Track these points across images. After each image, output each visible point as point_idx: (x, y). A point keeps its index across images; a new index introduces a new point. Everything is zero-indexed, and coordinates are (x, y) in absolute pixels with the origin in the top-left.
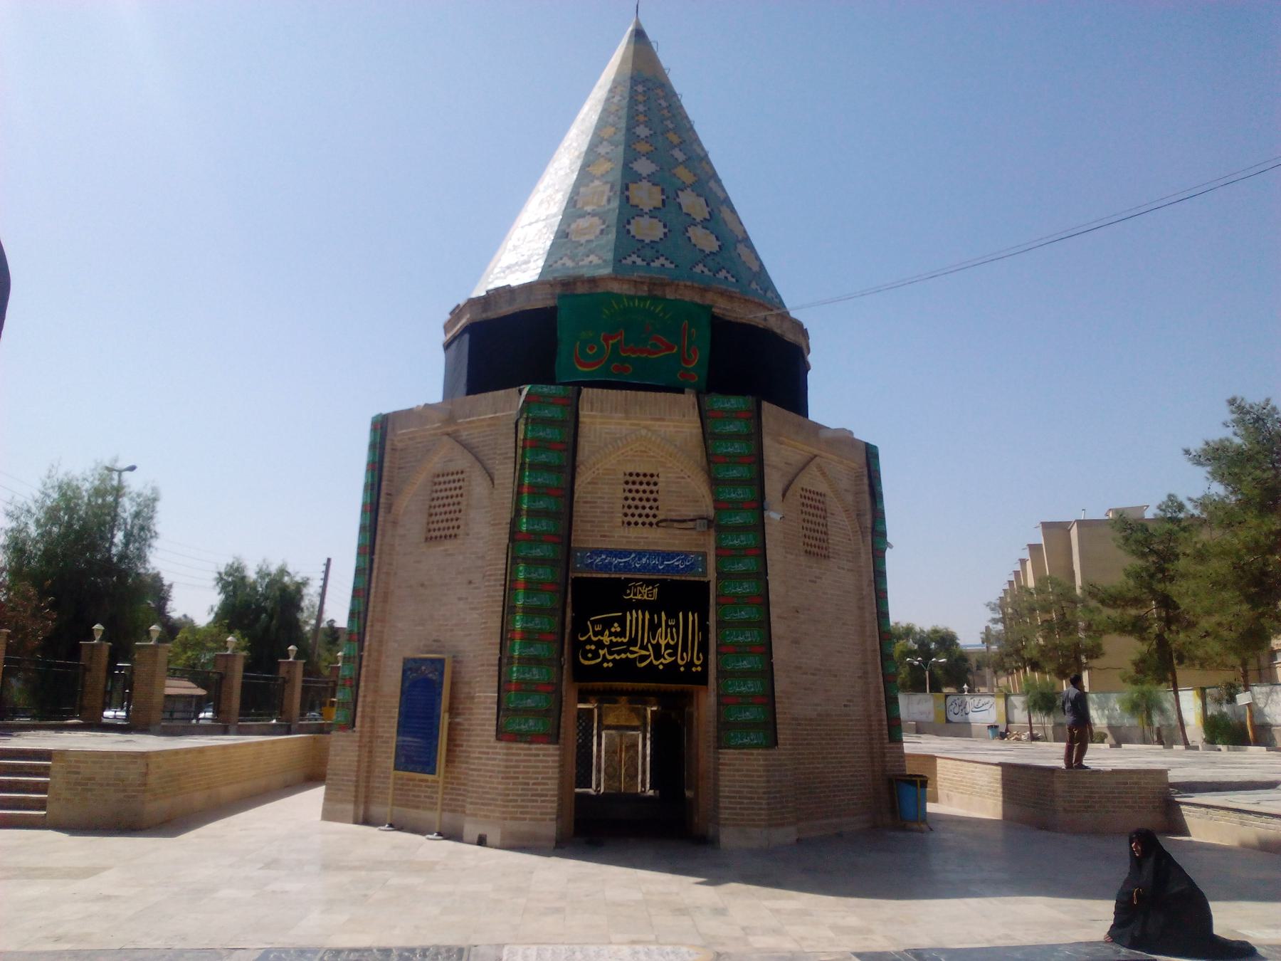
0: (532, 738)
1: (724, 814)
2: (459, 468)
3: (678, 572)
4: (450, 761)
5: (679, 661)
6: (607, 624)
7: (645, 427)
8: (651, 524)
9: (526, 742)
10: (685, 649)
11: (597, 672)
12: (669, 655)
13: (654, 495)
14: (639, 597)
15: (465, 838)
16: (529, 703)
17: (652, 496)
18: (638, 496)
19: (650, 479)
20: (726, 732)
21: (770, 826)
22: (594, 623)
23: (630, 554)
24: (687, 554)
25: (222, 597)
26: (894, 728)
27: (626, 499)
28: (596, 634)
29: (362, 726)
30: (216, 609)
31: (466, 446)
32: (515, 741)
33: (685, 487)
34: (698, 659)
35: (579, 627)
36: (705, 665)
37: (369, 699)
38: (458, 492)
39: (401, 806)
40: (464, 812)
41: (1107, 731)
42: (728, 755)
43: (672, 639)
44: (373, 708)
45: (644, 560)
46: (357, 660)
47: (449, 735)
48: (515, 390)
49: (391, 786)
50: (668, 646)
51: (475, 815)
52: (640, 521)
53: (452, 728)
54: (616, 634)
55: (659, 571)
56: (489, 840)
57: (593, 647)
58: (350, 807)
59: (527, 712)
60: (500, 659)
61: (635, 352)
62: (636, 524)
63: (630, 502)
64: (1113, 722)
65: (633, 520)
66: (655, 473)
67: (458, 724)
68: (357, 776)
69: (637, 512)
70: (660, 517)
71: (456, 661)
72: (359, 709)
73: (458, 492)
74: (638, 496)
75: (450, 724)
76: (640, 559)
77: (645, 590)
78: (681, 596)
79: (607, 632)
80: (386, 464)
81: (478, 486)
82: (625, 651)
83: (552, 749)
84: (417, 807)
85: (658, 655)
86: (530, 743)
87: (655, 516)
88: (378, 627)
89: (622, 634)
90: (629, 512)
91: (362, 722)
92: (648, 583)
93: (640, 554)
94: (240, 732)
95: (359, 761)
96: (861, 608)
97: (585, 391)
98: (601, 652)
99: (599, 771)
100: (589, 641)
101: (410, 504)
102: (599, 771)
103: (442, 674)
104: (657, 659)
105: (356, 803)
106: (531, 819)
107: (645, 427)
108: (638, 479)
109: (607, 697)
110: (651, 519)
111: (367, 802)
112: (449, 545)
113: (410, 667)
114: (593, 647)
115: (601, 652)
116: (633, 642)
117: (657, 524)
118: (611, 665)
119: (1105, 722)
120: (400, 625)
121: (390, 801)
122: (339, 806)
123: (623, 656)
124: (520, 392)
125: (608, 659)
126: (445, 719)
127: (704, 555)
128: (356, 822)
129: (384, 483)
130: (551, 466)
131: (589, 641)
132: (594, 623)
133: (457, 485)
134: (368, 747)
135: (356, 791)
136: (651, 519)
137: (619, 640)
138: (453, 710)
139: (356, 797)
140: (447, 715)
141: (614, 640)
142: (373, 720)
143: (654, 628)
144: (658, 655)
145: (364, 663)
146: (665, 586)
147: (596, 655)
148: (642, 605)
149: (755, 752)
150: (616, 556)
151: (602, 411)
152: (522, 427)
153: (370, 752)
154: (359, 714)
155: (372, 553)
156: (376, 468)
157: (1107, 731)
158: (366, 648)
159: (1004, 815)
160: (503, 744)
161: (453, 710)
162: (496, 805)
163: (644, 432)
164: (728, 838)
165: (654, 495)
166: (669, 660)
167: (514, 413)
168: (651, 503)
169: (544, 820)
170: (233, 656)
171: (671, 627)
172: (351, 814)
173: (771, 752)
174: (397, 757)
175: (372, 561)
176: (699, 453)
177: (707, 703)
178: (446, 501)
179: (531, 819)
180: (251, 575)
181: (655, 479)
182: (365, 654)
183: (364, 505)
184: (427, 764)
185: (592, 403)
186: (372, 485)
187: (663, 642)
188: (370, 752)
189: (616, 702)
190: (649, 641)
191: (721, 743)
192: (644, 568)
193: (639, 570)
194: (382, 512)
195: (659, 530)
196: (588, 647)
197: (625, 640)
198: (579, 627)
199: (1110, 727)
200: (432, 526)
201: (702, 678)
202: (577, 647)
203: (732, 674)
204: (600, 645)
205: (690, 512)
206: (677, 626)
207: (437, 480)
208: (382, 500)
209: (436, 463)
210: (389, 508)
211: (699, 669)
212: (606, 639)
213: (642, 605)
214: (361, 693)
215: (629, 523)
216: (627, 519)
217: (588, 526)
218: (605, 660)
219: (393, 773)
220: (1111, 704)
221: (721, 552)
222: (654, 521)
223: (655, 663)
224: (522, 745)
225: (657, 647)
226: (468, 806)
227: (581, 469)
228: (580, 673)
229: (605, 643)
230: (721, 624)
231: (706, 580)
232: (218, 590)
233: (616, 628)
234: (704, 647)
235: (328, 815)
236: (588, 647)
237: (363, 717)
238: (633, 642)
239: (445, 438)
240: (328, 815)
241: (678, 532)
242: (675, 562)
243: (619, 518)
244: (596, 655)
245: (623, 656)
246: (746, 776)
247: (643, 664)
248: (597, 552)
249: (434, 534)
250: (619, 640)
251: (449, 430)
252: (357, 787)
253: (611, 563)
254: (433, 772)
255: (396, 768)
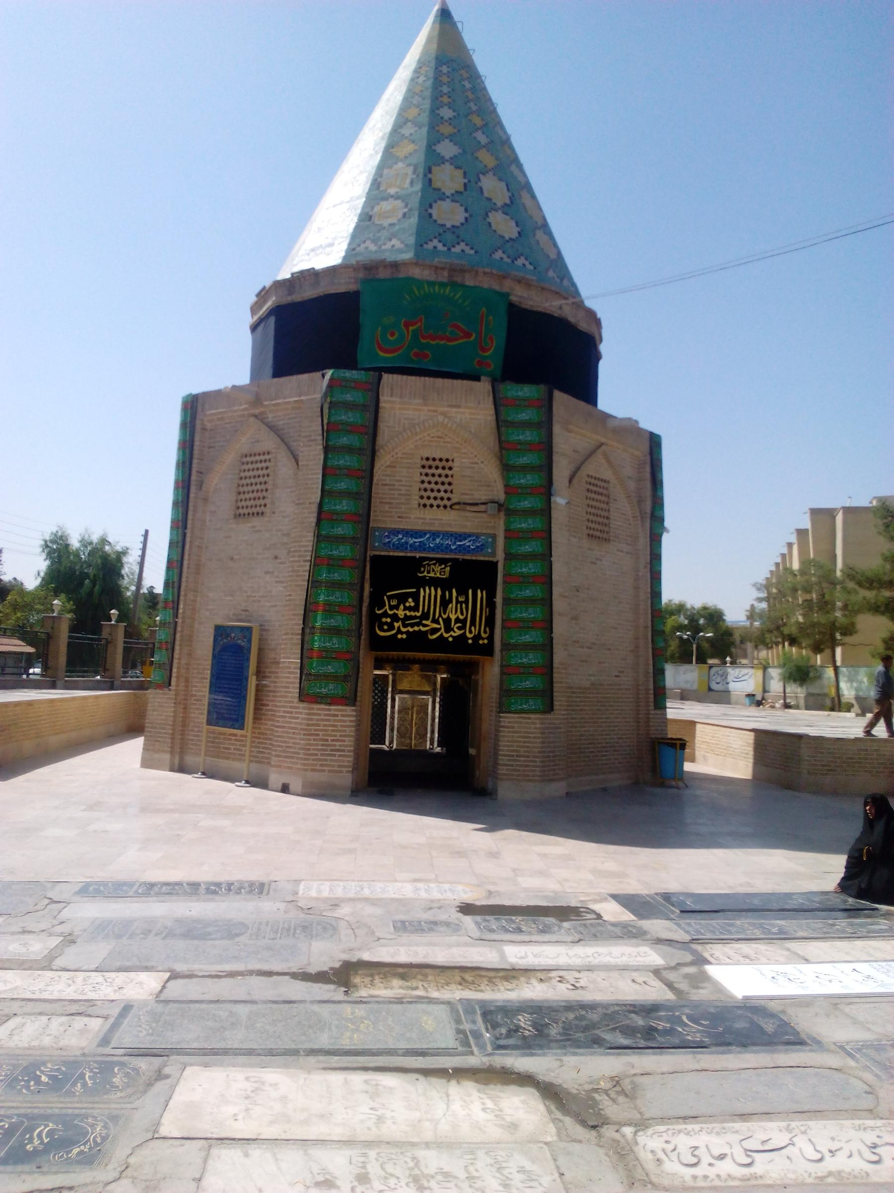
0: (332, 700)
1: (502, 770)
2: (266, 449)
3: (469, 552)
4: (257, 718)
5: (468, 635)
6: (402, 599)
7: (444, 414)
8: (445, 507)
9: (326, 704)
10: (473, 623)
11: (392, 643)
12: (459, 628)
13: (449, 479)
14: (432, 575)
15: (270, 785)
16: (330, 669)
17: (447, 480)
18: (433, 480)
19: (445, 463)
20: (507, 697)
21: (542, 781)
22: (389, 598)
23: (425, 534)
24: (478, 536)
25: (48, 562)
26: (660, 696)
27: (423, 482)
28: (392, 608)
29: (177, 686)
30: (42, 574)
31: (272, 428)
32: (316, 702)
33: (479, 472)
34: (485, 632)
35: (376, 601)
36: (491, 638)
37: (183, 661)
38: (265, 472)
39: (212, 756)
40: (269, 763)
41: (854, 702)
42: (508, 719)
43: (462, 614)
44: (188, 669)
45: (438, 540)
46: (172, 626)
47: (256, 695)
48: (319, 374)
49: (204, 739)
50: (457, 620)
51: (280, 766)
52: (435, 503)
53: (259, 689)
54: (410, 609)
55: (451, 550)
56: (291, 788)
57: (389, 620)
58: (167, 757)
59: (327, 677)
60: (303, 629)
61: (433, 338)
62: (432, 506)
63: (426, 485)
64: (860, 694)
65: (428, 502)
66: (450, 458)
67: (265, 686)
68: (174, 730)
69: (432, 495)
70: (454, 501)
71: (263, 629)
72: (174, 670)
73: (265, 472)
74: (433, 480)
75: (257, 685)
76: (434, 539)
77: (438, 568)
78: (472, 575)
79: (402, 607)
80: (197, 443)
81: (284, 468)
82: (418, 624)
83: (349, 710)
84: (227, 758)
85: (448, 629)
86: (330, 704)
87: (449, 499)
88: (191, 596)
89: (416, 608)
90: (425, 494)
91: (178, 681)
92: (441, 561)
93: (435, 535)
94: (68, 686)
95: (174, 717)
96: (636, 588)
97: (386, 377)
98: (396, 625)
99: (392, 730)
100: (385, 614)
101: (220, 482)
102: (392, 730)
103: (250, 641)
104: (447, 631)
105: (172, 753)
106: (330, 771)
107: (444, 414)
108: (434, 464)
109: (401, 665)
110: (445, 502)
111: (182, 752)
112: (256, 522)
113: (220, 632)
114: (389, 620)
115: (396, 625)
116: (425, 616)
117: (451, 507)
118: (404, 636)
119: (853, 693)
120: (211, 595)
121: (203, 753)
122: (157, 756)
123: (416, 628)
124: (323, 376)
125: (402, 631)
126: (252, 682)
127: (494, 537)
128: (172, 770)
129: (195, 461)
130: (352, 449)
131: (385, 614)
132: (390, 598)
133: (264, 465)
134: (183, 704)
135: (172, 743)
136: (445, 502)
137: (413, 614)
138: (259, 673)
139: (172, 747)
140: (254, 678)
141: (408, 614)
142: (187, 680)
143: (445, 603)
144: (448, 629)
145: (179, 629)
146: (458, 566)
147: (391, 627)
148: (434, 582)
149: (532, 716)
150: (412, 536)
151: (401, 397)
152: (326, 411)
153: (185, 708)
154: (174, 675)
155: (185, 527)
156: (187, 446)
157: (854, 702)
158: (180, 616)
159: (757, 777)
160: (305, 705)
161: (259, 673)
162: (298, 758)
163: (441, 418)
164: (505, 790)
165: (449, 479)
166: (458, 633)
167: (318, 396)
168: (446, 487)
169: (341, 772)
170: (58, 618)
171: (461, 603)
172: (168, 762)
173: (548, 716)
174: (209, 712)
175: (184, 535)
176: (492, 441)
177: (490, 674)
178: (253, 481)
179: (330, 771)
180: (75, 543)
181: (450, 463)
182: (179, 621)
183: (177, 483)
184: (237, 720)
185: (392, 389)
186: (184, 463)
187: (453, 617)
188: (185, 708)
189: (409, 669)
190: (440, 615)
191: (502, 708)
192: (438, 548)
193: (433, 550)
194: (193, 489)
195: (453, 513)
196: (384, 620)
197: (418, 614)
198: (376, 601)
199: (858, 698)
200: (240, 504)
201: (488, 650)
202: (374, 620)
203: (515, 647)
204: (395, 618)
205: (481, 495)
206: (467, 602)
207: (245, 460)
208: (194, 478)
209: (243, 443)
210: (200, 485)
211: (486, 641)
212: (401, 613)
213: (434, 582)
214: (176, 656)
215: (425, 506)
216: (423, 502)
217: (387, 507)
218: (399, 631)
219: (205, 727)
220: (860, 678)
221: (511, 535)
222: (448, 503)
223: (446, 635)
224: (323, 706)
225: (447, 621)
226: (274, 758)
227: (381, 453)
228: (376, 643)
229: (399, 616)
230: (507, 601)
231: (495, 560)
232: (44, 556)
233: (410, 603)
234: (490, 622)
235: (146, 763)
236: (384, 620)
237: (178, 677)
238: (425, 616)
239: (252, 419)
240: (146, 763)
241: (468, 514)
242: (466, 542)
243: (415, 500)
244: (391, 627)
245: (416, 628)
246: (523, 737)
247: (435, 636)
248: (395, 532)
249: (241, 511)
250: (413, 614)
251: (257, 411)
252: (173, 739)
253: (407, 543)
254: (241, 728)
255: (209, 723)
